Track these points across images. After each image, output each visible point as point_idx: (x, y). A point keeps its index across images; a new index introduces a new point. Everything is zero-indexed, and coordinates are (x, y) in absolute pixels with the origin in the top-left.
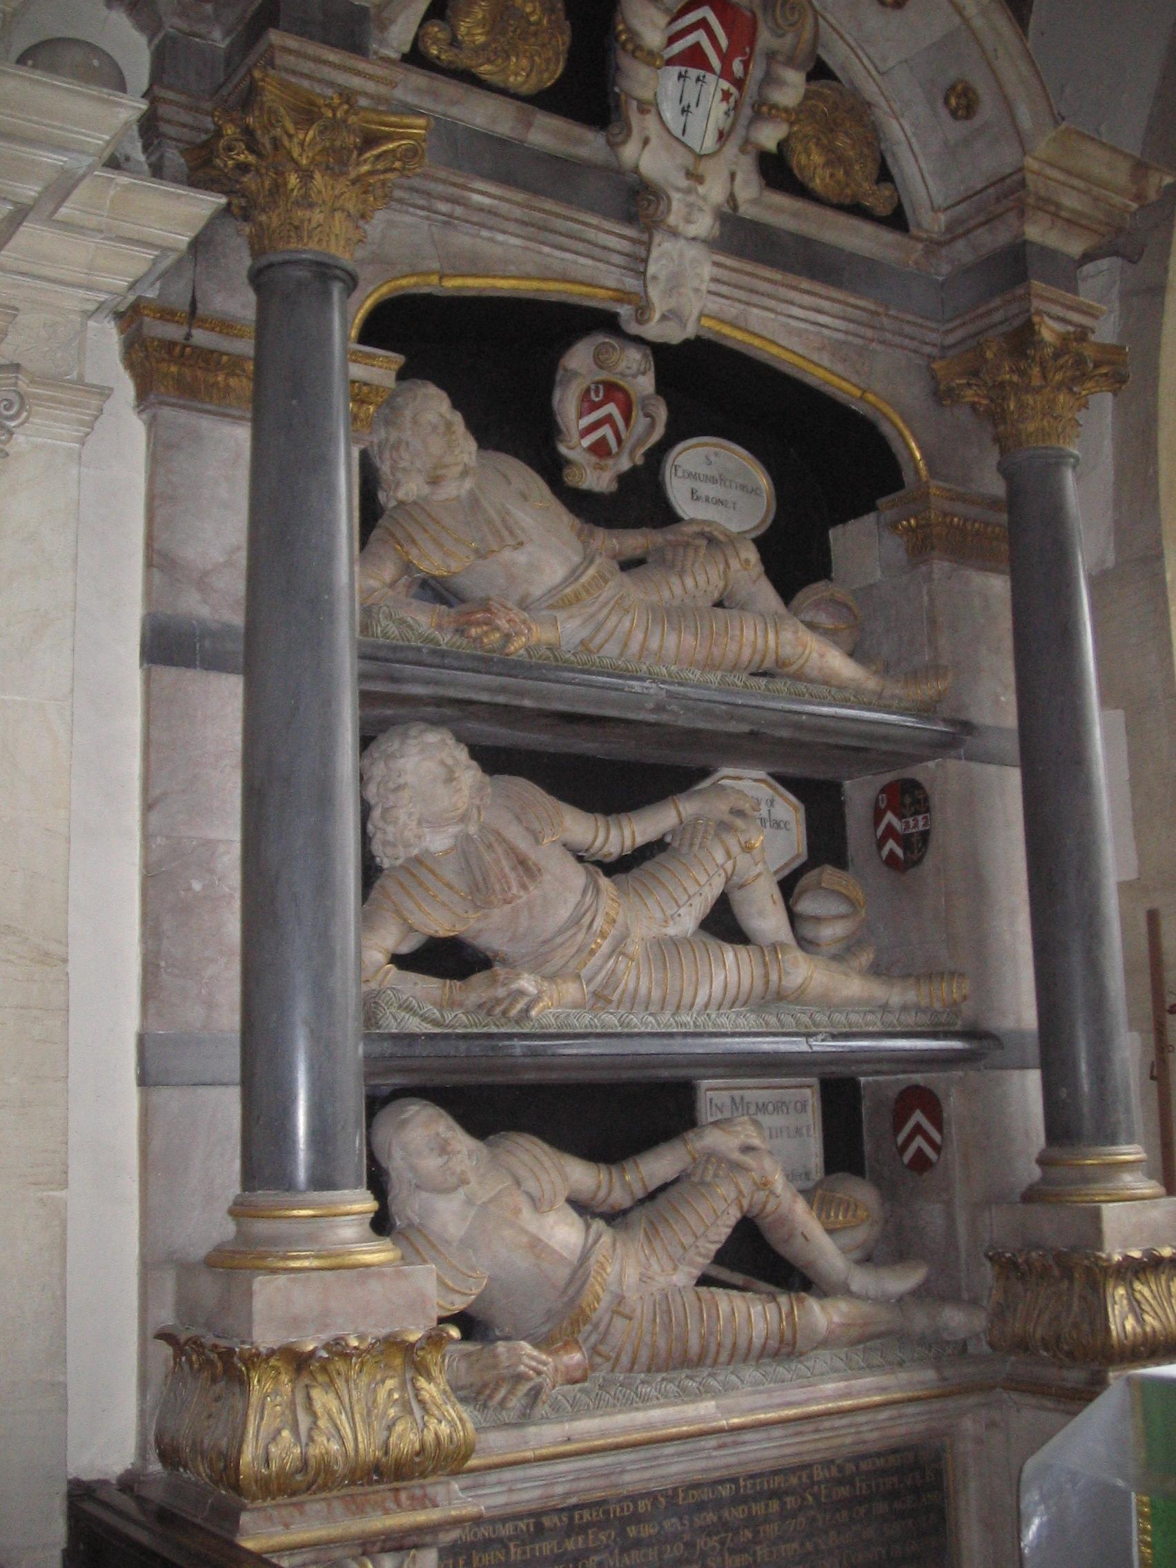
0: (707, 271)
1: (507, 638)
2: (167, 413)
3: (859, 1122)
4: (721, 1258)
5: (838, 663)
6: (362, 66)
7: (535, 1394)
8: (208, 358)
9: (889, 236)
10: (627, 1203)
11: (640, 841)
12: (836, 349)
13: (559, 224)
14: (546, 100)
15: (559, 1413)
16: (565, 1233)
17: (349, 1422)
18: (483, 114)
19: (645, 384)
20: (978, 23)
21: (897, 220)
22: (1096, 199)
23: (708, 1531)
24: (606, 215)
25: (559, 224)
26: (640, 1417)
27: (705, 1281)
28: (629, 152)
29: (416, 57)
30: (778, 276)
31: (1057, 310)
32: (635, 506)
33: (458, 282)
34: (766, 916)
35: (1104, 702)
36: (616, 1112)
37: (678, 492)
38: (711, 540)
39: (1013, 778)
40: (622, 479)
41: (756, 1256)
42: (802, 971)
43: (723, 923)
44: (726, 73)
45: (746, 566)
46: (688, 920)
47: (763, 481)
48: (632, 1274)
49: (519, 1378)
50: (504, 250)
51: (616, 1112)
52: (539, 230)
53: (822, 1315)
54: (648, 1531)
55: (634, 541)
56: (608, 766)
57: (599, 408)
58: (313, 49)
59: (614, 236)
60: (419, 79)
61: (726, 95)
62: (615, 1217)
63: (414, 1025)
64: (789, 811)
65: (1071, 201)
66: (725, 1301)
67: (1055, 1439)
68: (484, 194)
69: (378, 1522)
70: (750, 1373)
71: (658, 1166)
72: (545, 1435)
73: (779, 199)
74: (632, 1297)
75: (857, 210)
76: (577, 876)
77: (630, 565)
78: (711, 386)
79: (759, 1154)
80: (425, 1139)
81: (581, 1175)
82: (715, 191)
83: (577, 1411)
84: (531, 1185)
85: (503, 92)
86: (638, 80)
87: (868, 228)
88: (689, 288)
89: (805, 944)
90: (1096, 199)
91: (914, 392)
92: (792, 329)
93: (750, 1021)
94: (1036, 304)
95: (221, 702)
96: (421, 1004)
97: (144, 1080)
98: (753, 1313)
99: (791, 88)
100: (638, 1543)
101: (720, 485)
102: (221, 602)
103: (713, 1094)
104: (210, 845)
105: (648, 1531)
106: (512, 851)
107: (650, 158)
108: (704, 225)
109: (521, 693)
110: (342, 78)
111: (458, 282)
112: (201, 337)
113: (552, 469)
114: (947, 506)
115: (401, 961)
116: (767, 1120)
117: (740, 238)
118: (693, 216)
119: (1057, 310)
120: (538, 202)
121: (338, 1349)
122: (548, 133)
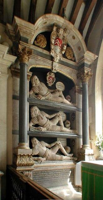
0: (58, 65)
1: (41, 98)
2: (14, 77)
3: (71, 143)
4: (57, 152)
5: (68, 102)
6: (27, 44)
7: (41, 161)
8: (16, 72)
9: (74, 63)
10: (50, 147)
11: (52, 117)
12: (69, 73)
13: (46, 61)
14: (45, 49)
15: (43, 163)
16: (45, 149)
17: (25, 161)
18: (40, 50)
19: (54, 76)
20: (81, 40)
21: (75, 61)
22: (91, 59)
23: (55, 174)
24: (49, 60)
25: (46, 61)
26: (49, 164)
27: (56, 154)
28: (51, 53)
29: (34, 44)
30: (64, 66)
31: (87, 70)
32: (53, 89)
33: (38, 66)
34: (62, 124)
35: (89, 107)
36: (51, 140)
37: (57, 87)
38: (59, 91)
39: (82, 113)
40: (52, 85)
41: (60, 152)
42: (64, 129)
43: (59, 124)
44: (59, 46)
45: (61, 93)
46: (56, 124)
47: (63, 85)
48: (50, 152)
49: (40, 160)
50: (43, 64)
51: (51, 140)
52: (44, 61)
53: (64, 157)
54: (50, 173)
55: (52, 91)
56: (51, 111)
57: (50, 78)
58: (23, 43)
59: (50, 62)
60: (34, 46)
61: (59, 48)
62: (49, 149)
63: (33, 131)
64: (65, 115)
65: (88, 59)
66: (57, 155)
67: (18, 141)
68: (40, 58)
69: (27, 169)
70: (58, 161)
71: (53, 145)
72: (42, 165)
73: (64, 59)
74: (50, 155)
75: (71, 60)
76: (46, 119)
77: (52, 93)
78: (59, 77)
79: (61, 144)
80: (36, 141)
81: (47, 145)
82: (58, 58)
83: (44, 163)
84: (42, 145)
85: (41, 48)
86: (53, 47)
87: (72, 62)
88: (57, 68)
89: (65, 127)
90: (91, 59)
91: (75, 77)
92: (66, 72)
93: (59, 132)
94: (85, 69)
95: (18, 102)
96: (33, 129)
97: (13, 134)
98: (59, 156)
99: (65, 47)
100: (49, 174)
101: (60, 86)
102: (18, 94)
103: (58, 139)
104: (17, 114)
105: (50, 173)
106: (41, 117)
107: (52, 54)
108: (57, 61)
109: (41, 103)
110: (25, 45)
111: (38, 66)
112: (16, 70)
113: (47, 85)
114: (77, 88)
115: (33, 126)
116: (62, 141)
117: (61, 62)
118: (57, 59)
119: (87, 70)
120: (44, 59)
121: (24, 155)
122: (45, 52)
